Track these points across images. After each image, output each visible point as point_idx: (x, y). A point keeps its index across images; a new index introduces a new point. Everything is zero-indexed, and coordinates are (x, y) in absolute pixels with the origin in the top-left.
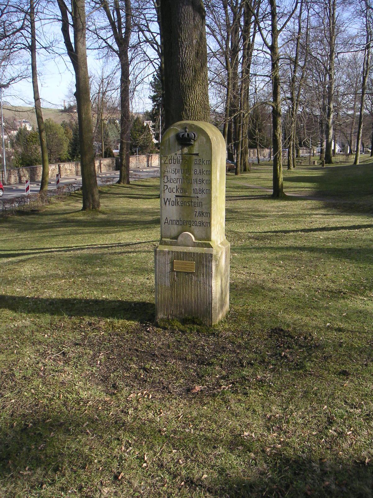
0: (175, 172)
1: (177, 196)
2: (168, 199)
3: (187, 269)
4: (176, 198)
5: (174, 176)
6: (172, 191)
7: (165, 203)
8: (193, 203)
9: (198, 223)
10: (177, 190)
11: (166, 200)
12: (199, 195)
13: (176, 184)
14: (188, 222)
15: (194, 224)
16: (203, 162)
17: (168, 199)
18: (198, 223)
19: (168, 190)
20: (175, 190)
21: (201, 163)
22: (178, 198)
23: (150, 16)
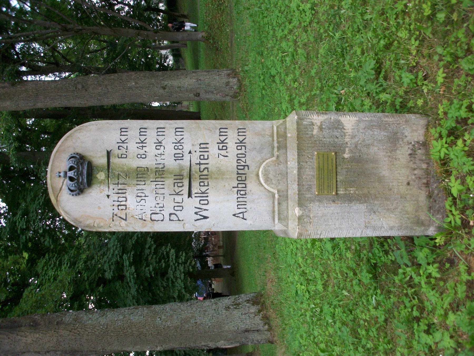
0: (141, 197)
1: (190, 195)
2: (196, 213)
3: (330, 167)
4: (193, 196)
5: (31, 122)
6: (180, 206)
7: (205, 218)
8: (203, 162)
9: (240, 152)
10: (177, 194)
11: (199, 217)
12: (186, 150)
13: (167, 195)
14: (240, 172)
15: (243, 159)
16: (123, 142)
17: (196, 213)
18: (240, 152)
19: (177, 213)
20: (178, 199)
21: (125, 145)
22: (194, 191)
23: (324, 234)
